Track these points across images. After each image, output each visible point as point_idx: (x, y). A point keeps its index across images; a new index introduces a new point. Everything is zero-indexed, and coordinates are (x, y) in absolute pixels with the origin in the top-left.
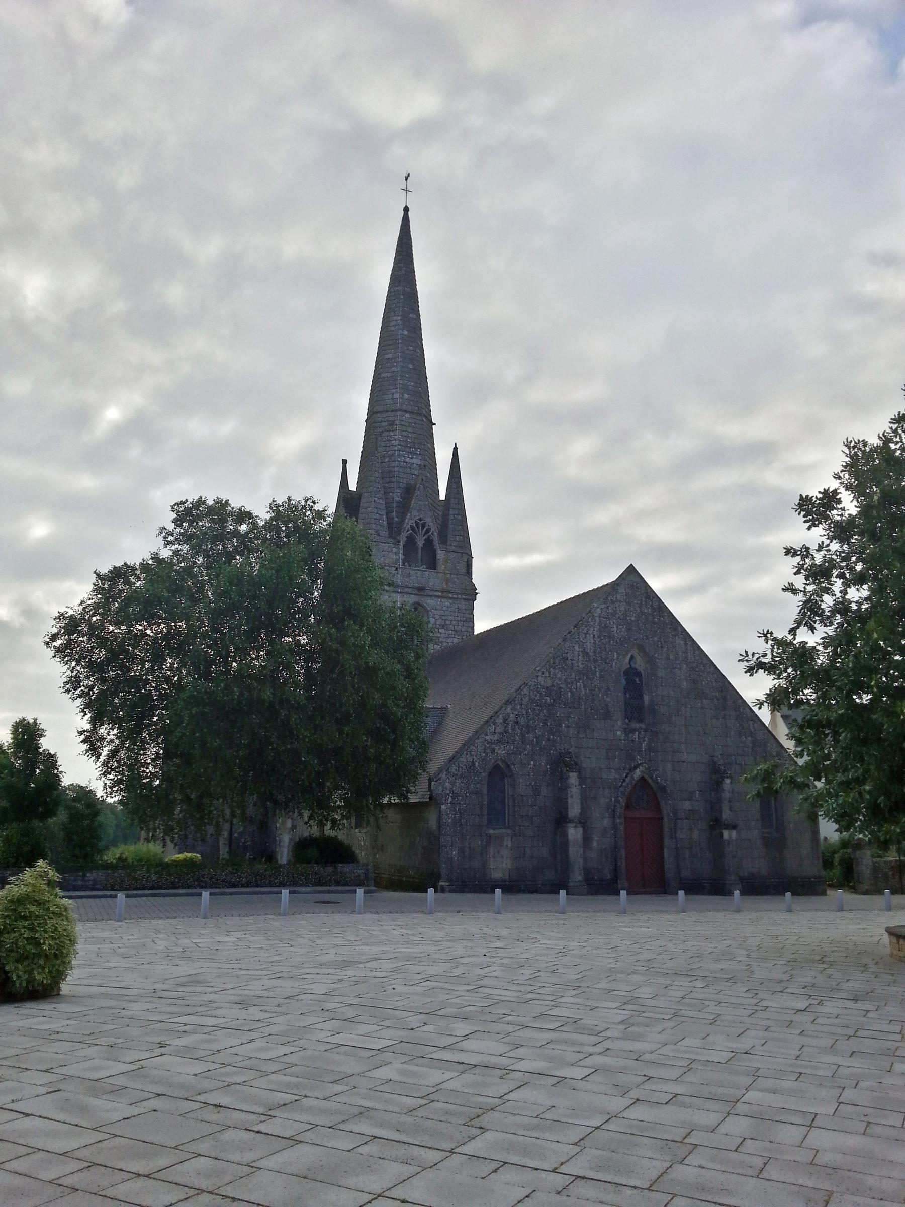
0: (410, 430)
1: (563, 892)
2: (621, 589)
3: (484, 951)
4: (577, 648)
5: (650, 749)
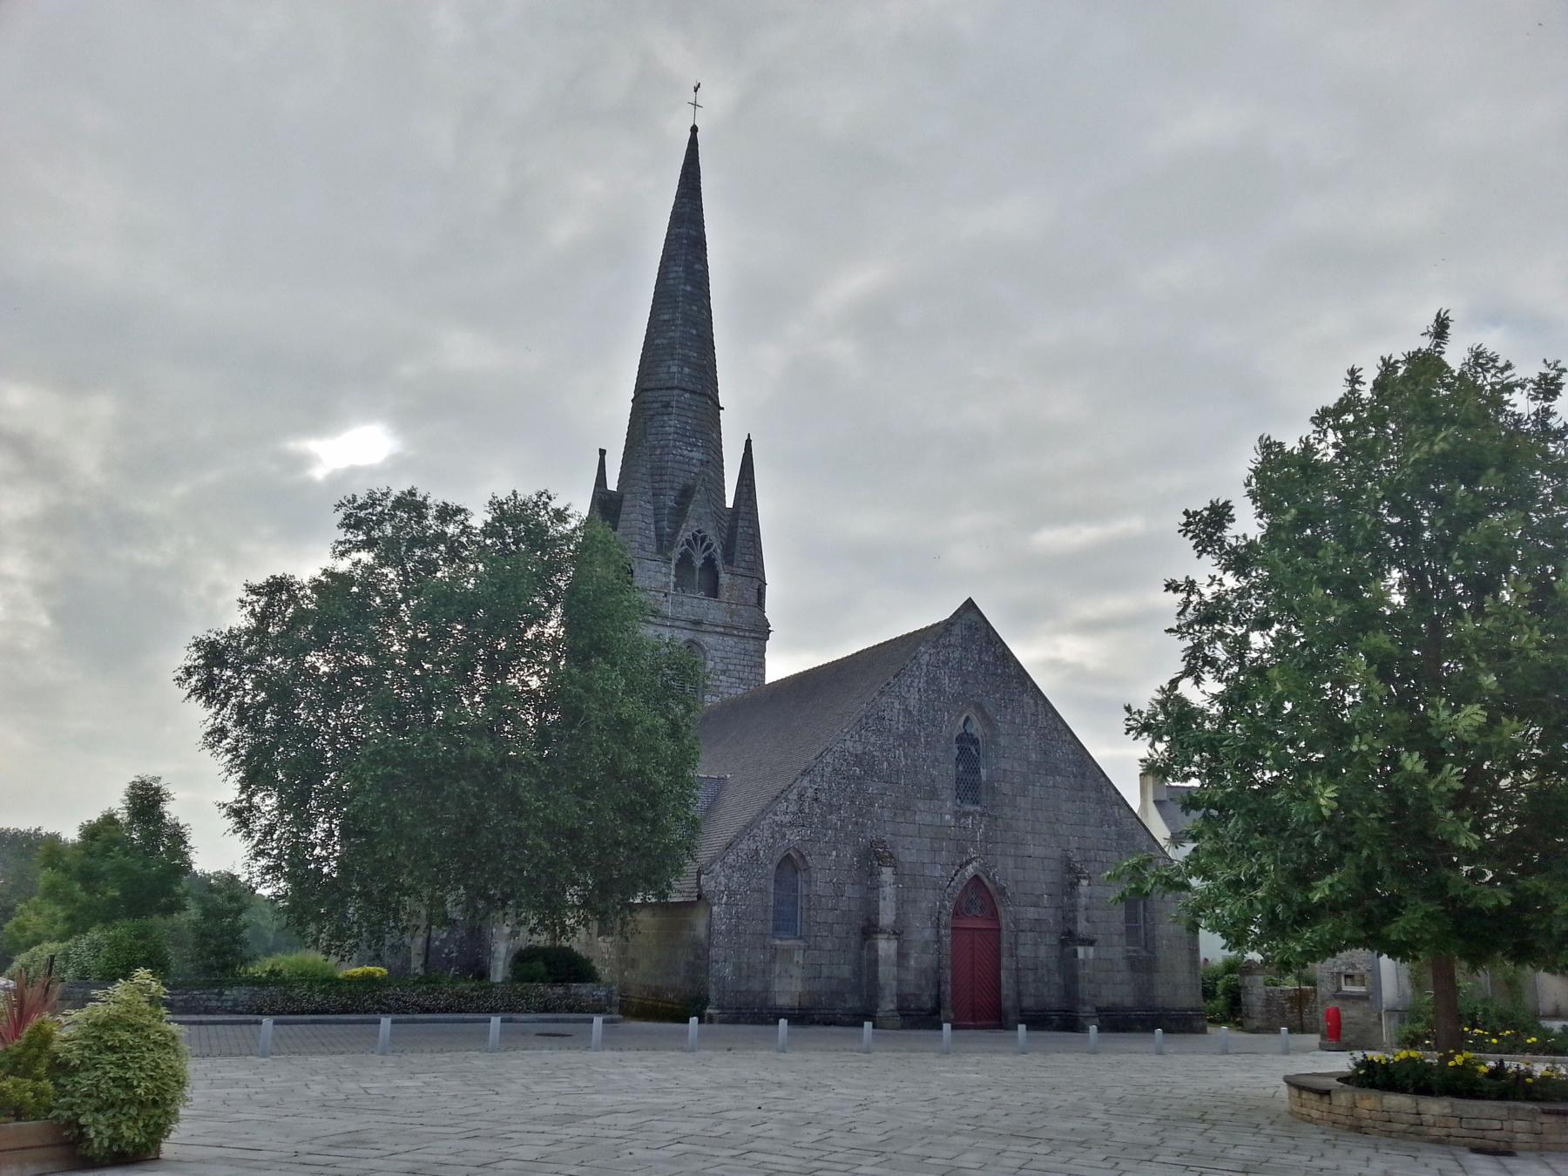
0: (690, 414)
1: (868, 1025)
2: (956, 630)
3: (759, 1102)
4: (897, 705)
5: (986, 839)
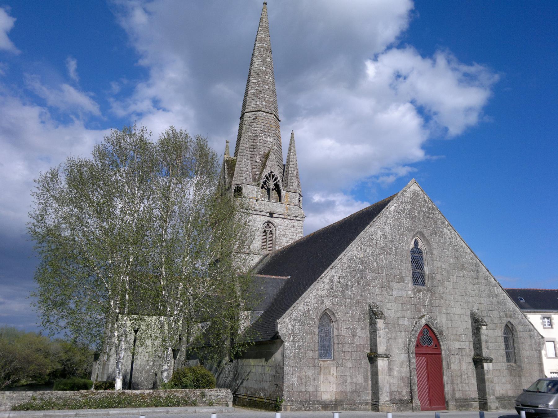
5: (431, 305)
